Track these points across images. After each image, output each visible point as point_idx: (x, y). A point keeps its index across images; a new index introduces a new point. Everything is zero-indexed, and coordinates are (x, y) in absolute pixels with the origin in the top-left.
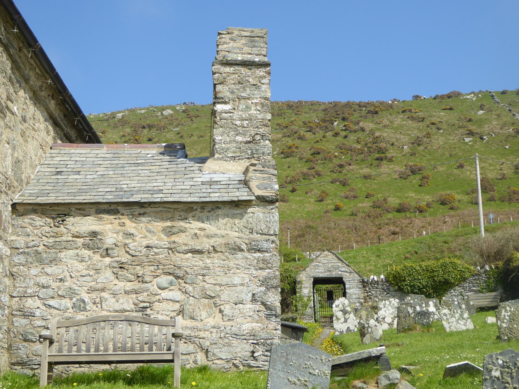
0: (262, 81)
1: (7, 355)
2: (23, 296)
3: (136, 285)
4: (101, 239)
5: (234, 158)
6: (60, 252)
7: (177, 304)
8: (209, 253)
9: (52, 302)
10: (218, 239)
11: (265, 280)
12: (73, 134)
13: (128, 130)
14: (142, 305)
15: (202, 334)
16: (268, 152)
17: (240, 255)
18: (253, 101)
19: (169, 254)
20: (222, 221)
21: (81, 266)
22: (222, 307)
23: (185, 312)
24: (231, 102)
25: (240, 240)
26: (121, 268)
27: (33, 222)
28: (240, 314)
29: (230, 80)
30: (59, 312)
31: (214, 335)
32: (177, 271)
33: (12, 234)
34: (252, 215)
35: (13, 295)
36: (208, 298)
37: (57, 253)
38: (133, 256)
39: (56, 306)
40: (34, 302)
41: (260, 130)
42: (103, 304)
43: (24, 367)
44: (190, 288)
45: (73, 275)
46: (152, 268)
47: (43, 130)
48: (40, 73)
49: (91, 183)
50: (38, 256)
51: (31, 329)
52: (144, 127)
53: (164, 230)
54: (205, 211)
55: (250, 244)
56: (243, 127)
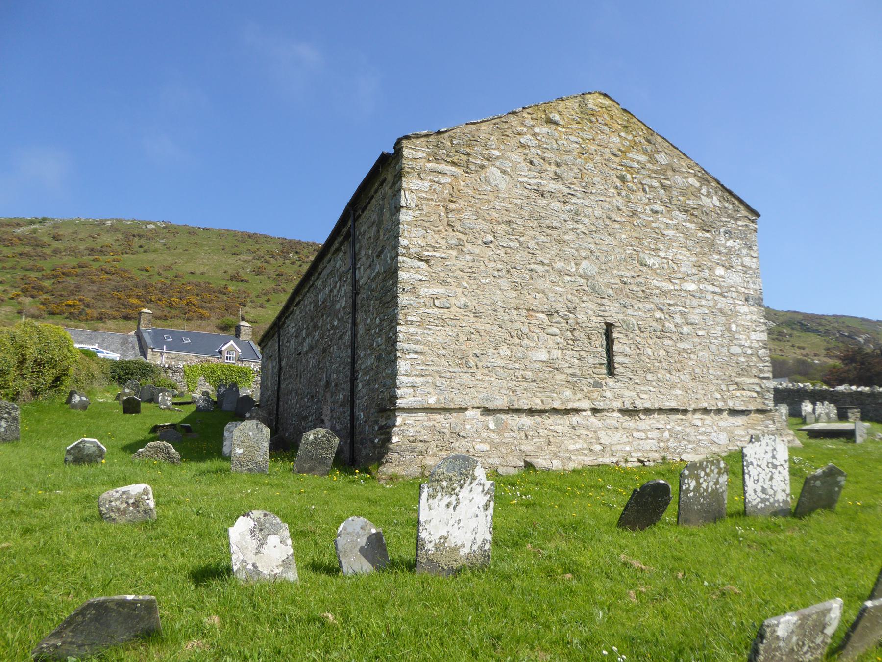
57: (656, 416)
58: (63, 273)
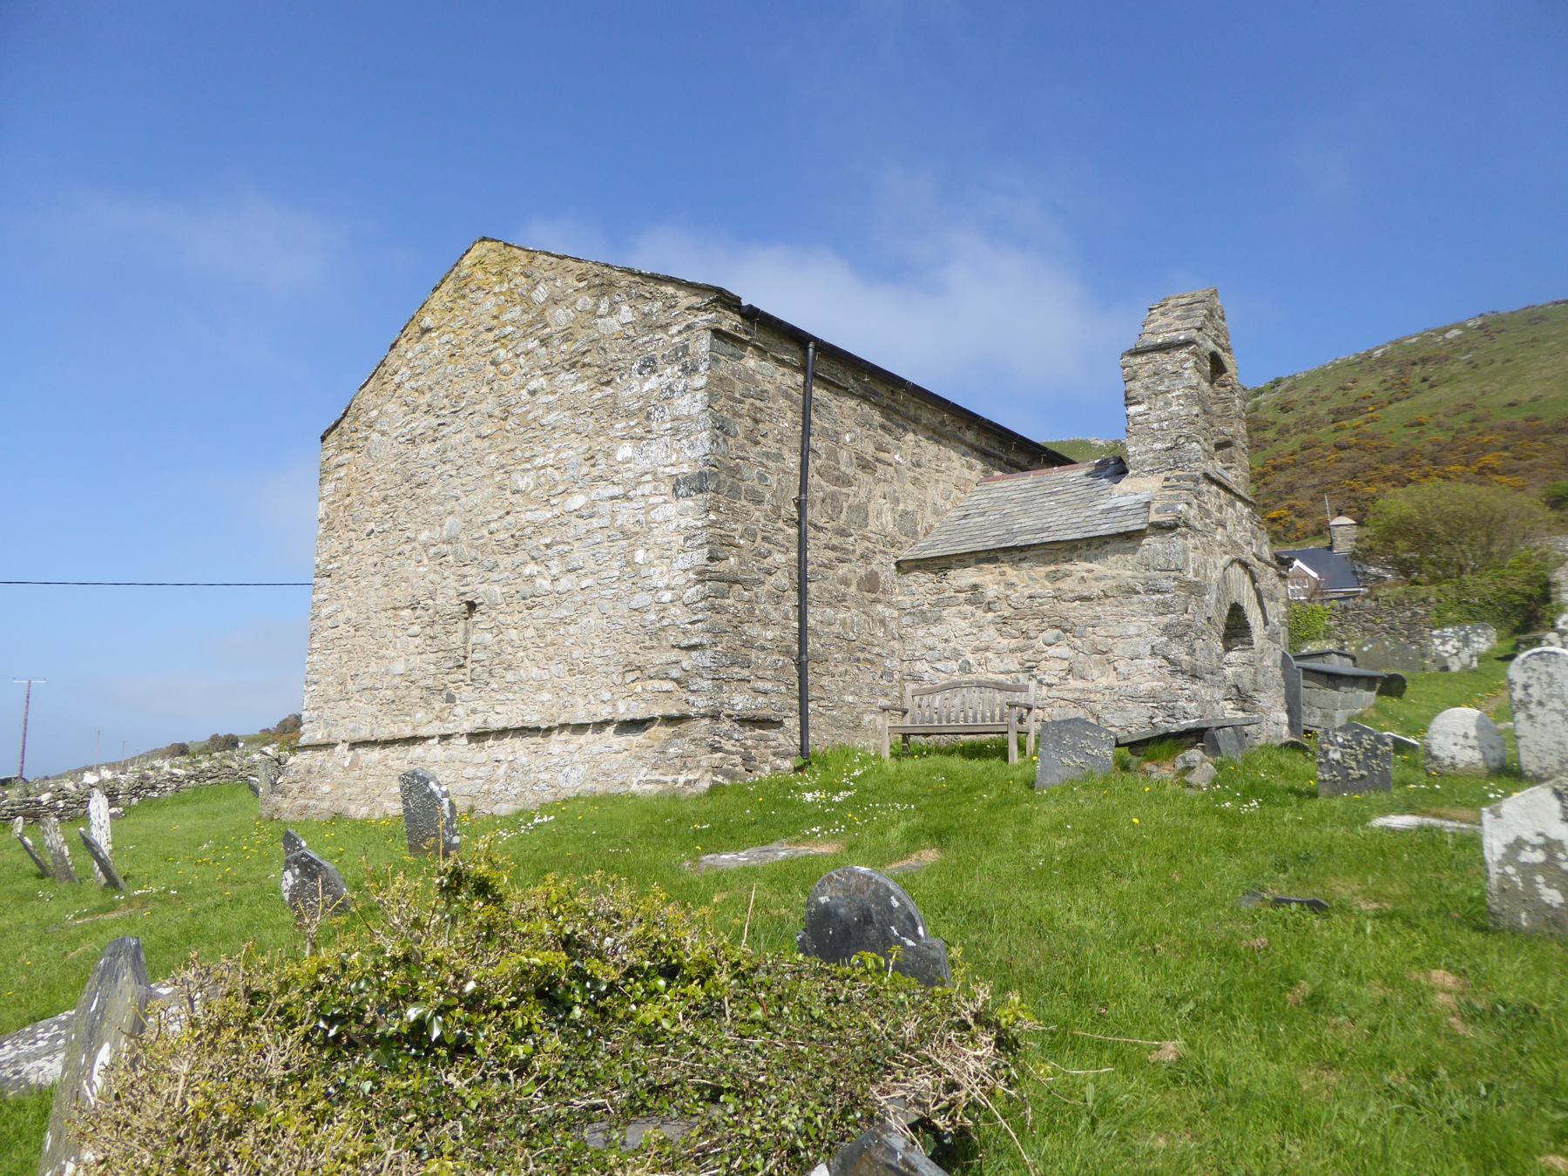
2: (912, 660)
3: (1020, 642)
9: (938, 665)
13: (1391, 372)
15: (1092, 697)
17: (1136, 598)
20: (1112, 559)
21: (963, 624)
29: (1143, 373)
44: (1078, 642)
52: (1414, 364)
57: (490, 742)
58: (1275, 468)
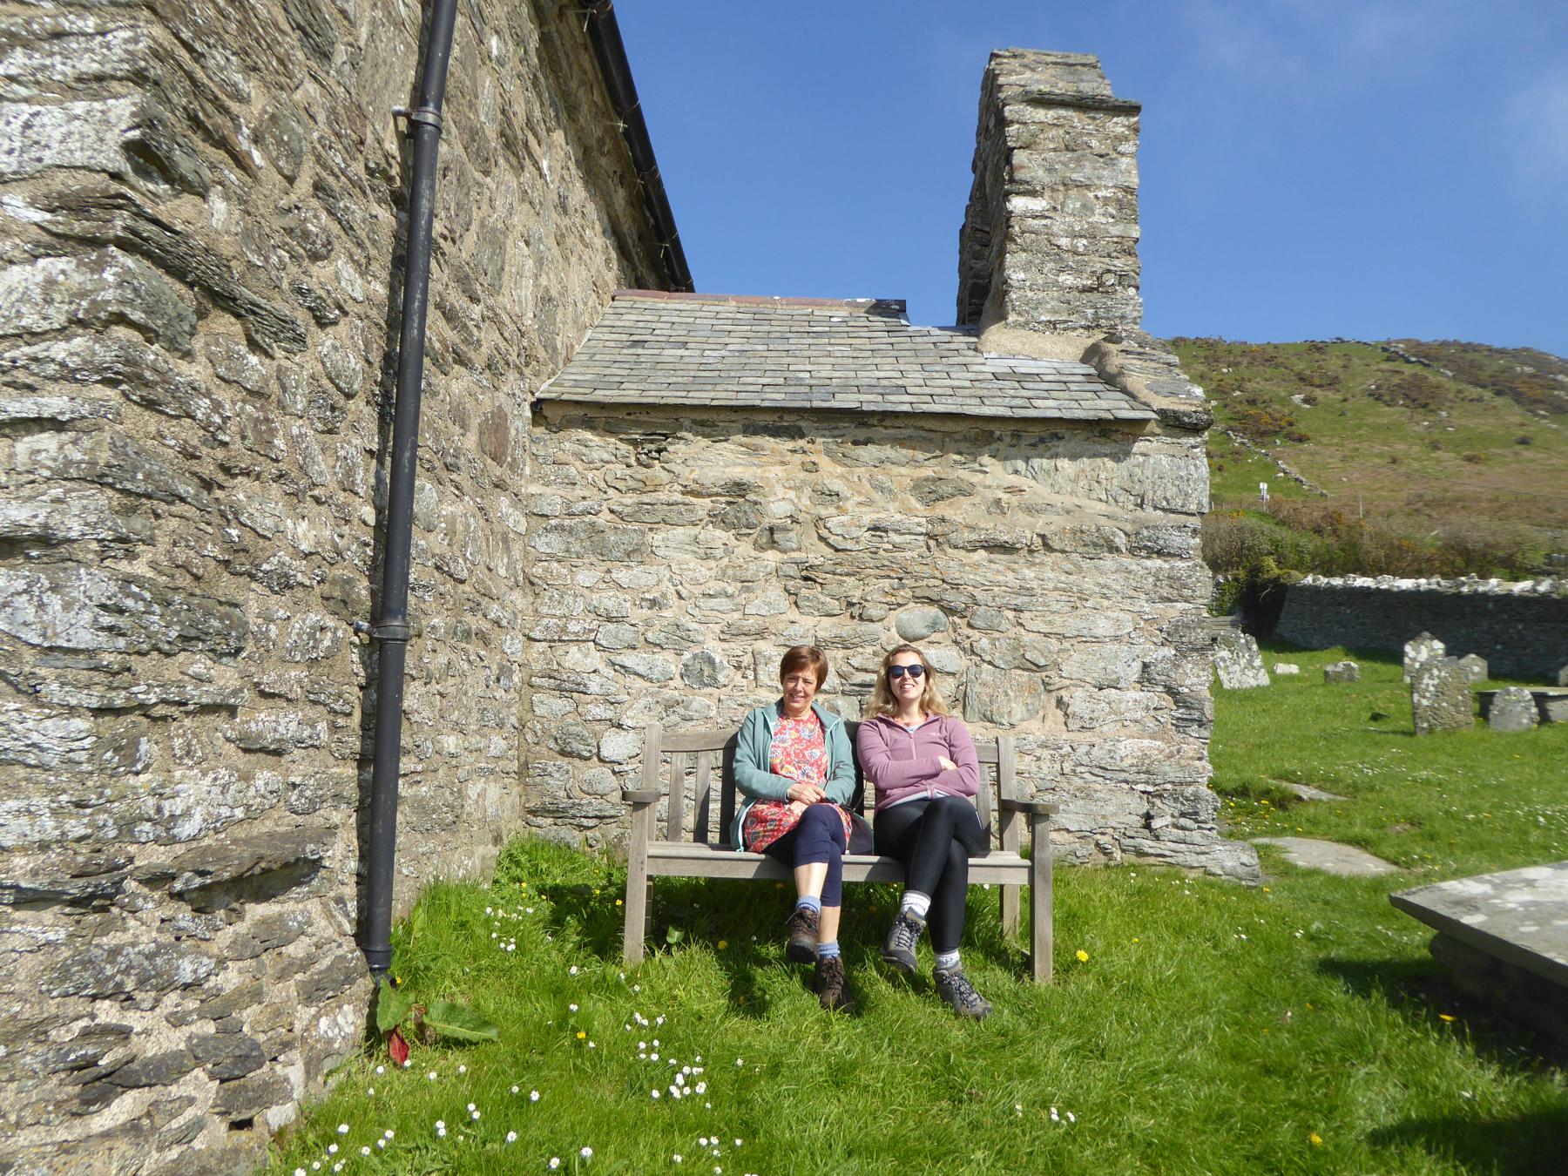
0: (1121, 149)
1: (516, 790)
4: (756, 503)
5: (1053, 325)
6: (651, 530)
7: (950, 679)
8: (1031, 552)
9: (629, 659)
10: (1055, 518)
11: (1176, 630)
12: (651, 279)
14: (860, 677)
16: (1135, 314)
17: (1109, 562)
18: (1100, 194)
19: (929, 548)
21: (704, 571)
22: (1063, 693)
23: (970, 701)
24: (1047, 193)
25: (1110, 523)
26: (806, 579)
27: (584, 450)
28: (1109, 714)
30: (648, 684)
31: (1045, 766)
32: (950, 596)
33: (532, 480)
34: (1141, 459)
35: (532, 635)
36: (1028, 670)
37: (643, 533)
38: (837, 550)
39: (641, 670)
40: (586, 656)
41: (1116, 262)
42: (760, 672)
43: (559, 821)
45: (684, 593)
46: (886, 584)
47: (597, 257)
48: (600, 103)
49: (720, 366)
50: (595, 538)
51: (577, 725)
53: (917, 486)
54: (1023, 443)
55: (1137, 534)
56: (1076, 253)
